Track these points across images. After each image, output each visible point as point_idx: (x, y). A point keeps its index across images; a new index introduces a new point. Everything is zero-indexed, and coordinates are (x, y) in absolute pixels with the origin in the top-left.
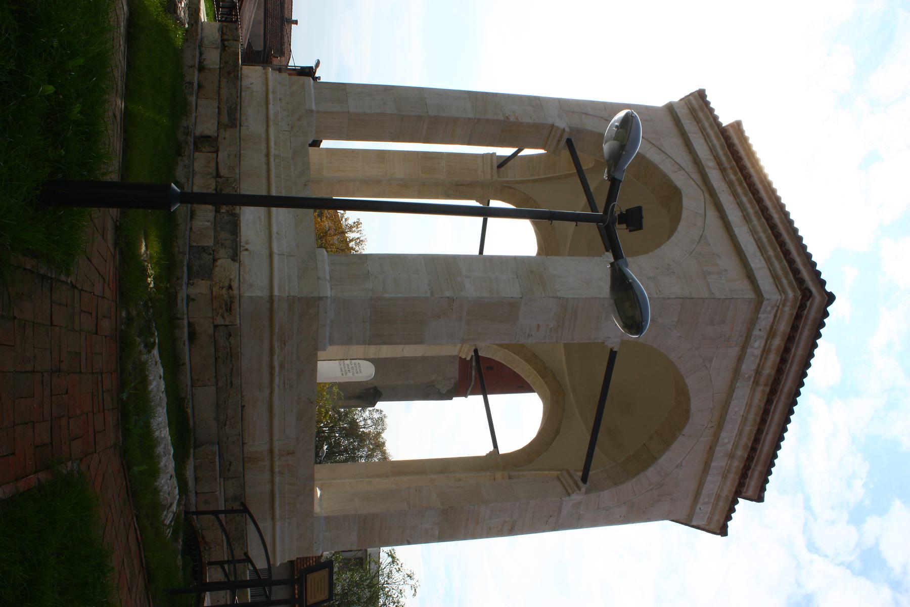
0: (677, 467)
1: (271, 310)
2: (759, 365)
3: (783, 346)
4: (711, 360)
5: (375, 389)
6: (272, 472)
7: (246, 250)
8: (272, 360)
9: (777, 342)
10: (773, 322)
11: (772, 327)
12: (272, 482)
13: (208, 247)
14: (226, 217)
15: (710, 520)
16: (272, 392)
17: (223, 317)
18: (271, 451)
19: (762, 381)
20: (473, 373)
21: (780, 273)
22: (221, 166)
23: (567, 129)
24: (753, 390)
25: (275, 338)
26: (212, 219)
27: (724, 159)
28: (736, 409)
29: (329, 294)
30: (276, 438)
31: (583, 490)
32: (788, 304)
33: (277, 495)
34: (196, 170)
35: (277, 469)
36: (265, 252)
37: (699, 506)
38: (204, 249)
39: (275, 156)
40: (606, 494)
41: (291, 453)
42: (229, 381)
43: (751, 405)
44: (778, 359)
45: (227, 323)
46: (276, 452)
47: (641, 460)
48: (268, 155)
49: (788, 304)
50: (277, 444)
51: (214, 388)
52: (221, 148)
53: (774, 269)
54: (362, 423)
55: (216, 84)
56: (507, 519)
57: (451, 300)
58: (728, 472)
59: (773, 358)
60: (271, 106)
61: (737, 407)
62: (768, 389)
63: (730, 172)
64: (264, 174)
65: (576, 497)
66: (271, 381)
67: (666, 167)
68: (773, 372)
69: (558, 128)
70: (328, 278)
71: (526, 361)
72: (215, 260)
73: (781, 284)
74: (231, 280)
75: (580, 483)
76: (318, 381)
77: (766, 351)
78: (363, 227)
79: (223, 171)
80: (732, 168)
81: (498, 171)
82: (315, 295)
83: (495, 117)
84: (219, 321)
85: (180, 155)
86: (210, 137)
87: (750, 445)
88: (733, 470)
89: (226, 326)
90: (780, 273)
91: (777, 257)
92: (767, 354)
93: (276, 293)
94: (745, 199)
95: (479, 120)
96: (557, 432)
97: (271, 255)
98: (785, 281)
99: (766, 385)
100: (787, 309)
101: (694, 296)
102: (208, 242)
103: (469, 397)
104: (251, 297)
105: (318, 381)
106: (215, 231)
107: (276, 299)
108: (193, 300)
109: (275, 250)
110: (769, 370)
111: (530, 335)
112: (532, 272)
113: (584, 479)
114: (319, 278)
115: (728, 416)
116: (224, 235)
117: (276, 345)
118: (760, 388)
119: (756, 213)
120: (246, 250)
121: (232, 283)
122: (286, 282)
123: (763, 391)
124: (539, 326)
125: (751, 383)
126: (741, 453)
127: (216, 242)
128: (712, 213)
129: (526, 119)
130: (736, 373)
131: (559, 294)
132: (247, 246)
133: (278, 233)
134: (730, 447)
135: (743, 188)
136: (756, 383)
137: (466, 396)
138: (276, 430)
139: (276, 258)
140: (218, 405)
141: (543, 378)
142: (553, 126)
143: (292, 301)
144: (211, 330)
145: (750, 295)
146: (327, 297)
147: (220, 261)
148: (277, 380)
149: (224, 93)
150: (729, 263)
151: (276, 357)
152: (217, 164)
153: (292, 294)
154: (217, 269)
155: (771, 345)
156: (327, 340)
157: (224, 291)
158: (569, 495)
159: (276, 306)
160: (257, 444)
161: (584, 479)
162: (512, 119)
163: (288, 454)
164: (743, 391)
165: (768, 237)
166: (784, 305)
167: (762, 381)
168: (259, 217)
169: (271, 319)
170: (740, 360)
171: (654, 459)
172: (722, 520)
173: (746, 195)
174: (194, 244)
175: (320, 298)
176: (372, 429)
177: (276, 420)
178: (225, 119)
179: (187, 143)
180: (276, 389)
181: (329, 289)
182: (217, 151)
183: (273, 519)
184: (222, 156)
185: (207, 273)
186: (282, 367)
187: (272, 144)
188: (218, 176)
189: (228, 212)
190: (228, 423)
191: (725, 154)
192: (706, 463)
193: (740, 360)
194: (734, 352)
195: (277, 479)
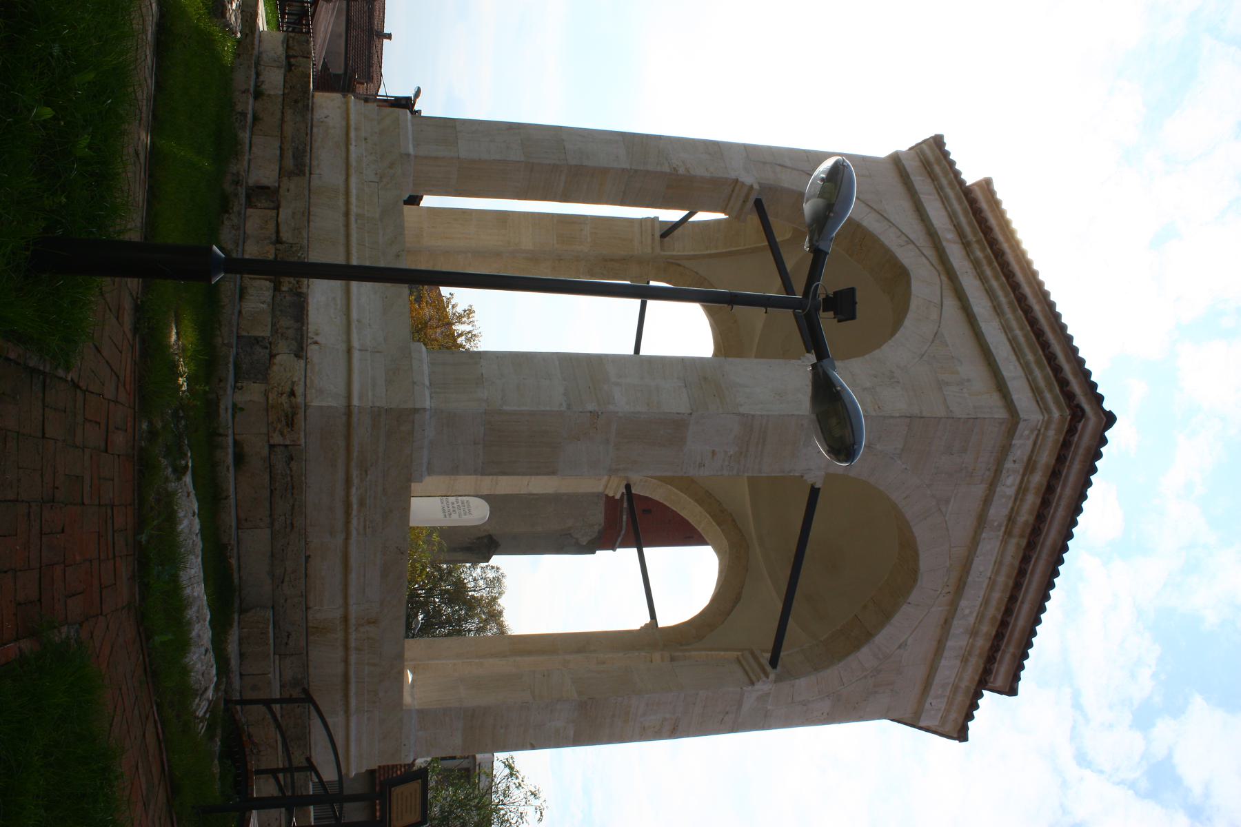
0: (899, 647)
1: (349, 425)
2: (1012, 509)
3: (1045, 484)
4: (947, 501)
5: (490, 537)
6: (346, 648)
7: (316, 343)
8: (348, 495)
9: (1038, 478)
10: (1032, 451)
11: (1030, 459)
12: (346, 661)
13: (264, 338)
14: (288, 298)
15: (944, 720)
16: (347, 539)
17: (282, 434)
18: (345, 619)
19: (1017, 531)
20: (625, 517)
21: (1042, 384)
22: (283, 228)
23: (756, 186)
24: (1004, 542)
25: (353, 464)
26: (269, 300)
27: (967, 230)
28: (982, 569)
29: (427, 404)
30: (352, 601)
31: (772, 677)
32: (1053, 426)
33: (353, 680)
34: (249, 232)
35: (353, 644)
36: (342, 347)
37: (929, 700)
38: (257, 340)
39: (357, 215)
40: (802, 682)
41: (374, 622)
42: (289, 522)
43: (1001, 563)
44: (1039, 501)
45: (288, 442)
46: (352, 621)
47: (853, 636)
48: (347, 214)
49: (1053, 426)
50: (353, 610)
51: (268, 531)
52: (283, 203)
53: (1034, 380)
54: (472, 584)
55: (279, 115)
56: (668, 716)
57: (595, 415)
58: (970, 654)
59: (1031, 500)
60: (352, 148)
61: (983, 566)
62: (1024, 542)
63: (976, 247)
64: (342, 239)
65: (762, 687)
66: (347, 522)
67: (890, 239)
68: (1031, 519)
69: (743, 183)
70: (427, 383)
71: (696, 501)
72: (272, 356)
73: (1043, 398)
74: (293, 383)
75: (769, 668)
76: (411, 525)
77: (1022, 490)
78: (476, 317)
79: (286, 235)
80: (978, 242)
81: (661, 242)
82: (409, 405)
83: (659, 169)
84: (277, 439)
85: (227, 212)
86: (268, 188)
87: (999, 617)
88: (977, 652)
89: (286, 446)
90: (1042, 384)
91: (1038, 362)
92: (1024, 494)
93: (355, 402)
94: (995, 284)
95: (636, 171)
96: (738, 599)
97: (349, 351)
98: (1048, 396)
99: (1022, 536)
100: (1051, 433)
101: (924, 414)
102: (264, 332)
103: (619, 550)
104: (321, 407)
105: (411, 525)
106: (274, 316)
107: (355, 411)
108: (242, 409)
109: (356, 344)
110: (1025, 516)
111: (702, 465)
112: (705, 379)
113: (774, 662)
114: (414, 383)
115: (970, 579)
116: (285, 322)
117: (355, 473)
118: (1014, 541)
119: (1010, 303)
120: (316, 343)
121: (296, 388)
122: (370, 389)
123: (1018, 544)
124: (714, 453)
125: (1001, 533)
126: (987, 629)
127: (275, 331)
128: (951, 304)
129: (699, 172)
130: (981, 520)
131: (742, 410)
132: (316, 338)
133: (359, 321)
134: (972, 620)
135: (993, 269)
136: (1008, 533)
137: (614, 549)
138: (352, 590)
139: (356, 355)
140: (272, 555)
141: (719, 524)
142: (737, 181)
143: (377, 414)
144: (266, 451)
145: (1001, 414)
146: (424, 409)
147: (279, 358)
148: (354, 522)
149: (289, 129)
150: (972, 370)
151: (354, 490)
152: (278, 225)
153: (378, 404)
154: (275, 368)
155: (1028, 482)
156: (424, 468)
157: (284, 399)
158: (752, 683)
159: (355, 419)
160: (327, 609)
161: (774, 662)
162: (681, 171)
163: (369, 623)
164: (990, 546)
165: (1026, 336)
166: (1047, 428)
167: (1017, 531)
168: (334, 299)
169: (348, 437)
170: (987, 501)
171: (869, 636)
172: (960, 720)
173: (997, 278)
174: (245, 334)
175: (416, 411)
176: (484, 593)
177: (353, 576)
178: (289, 163)
179: (236, 195)
180: (354, 533)
181: (428, 398)
182: (277, 208)
183: (347, 711)
184: (285, 213)
185: (262, 373)
186: (362, 503)
187: (353, 200)
188: (278, 241)
189: (291, 290)
190: (287, 579)
191: (970, 223)
192: (939, 641)
193: (987, 501)
194: (979, 490)
195: (353, 658)
